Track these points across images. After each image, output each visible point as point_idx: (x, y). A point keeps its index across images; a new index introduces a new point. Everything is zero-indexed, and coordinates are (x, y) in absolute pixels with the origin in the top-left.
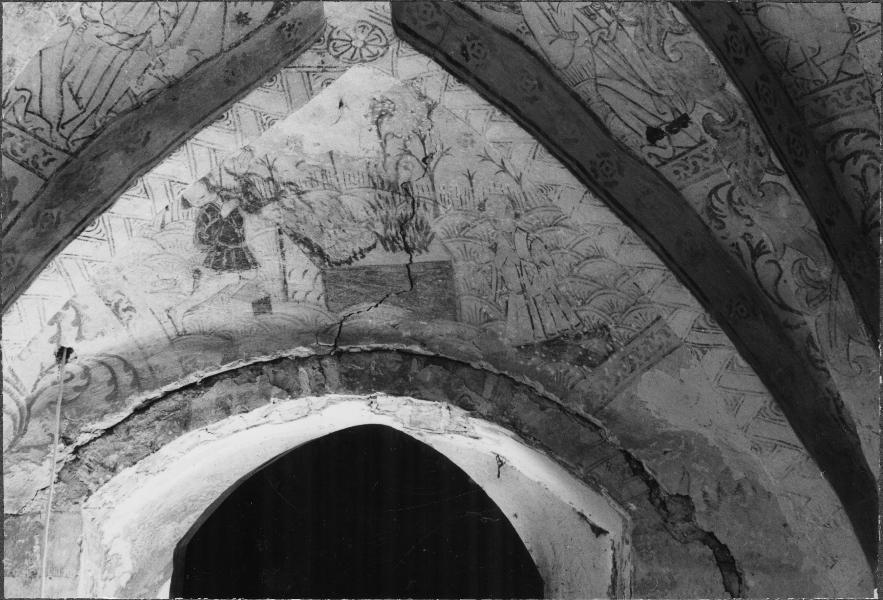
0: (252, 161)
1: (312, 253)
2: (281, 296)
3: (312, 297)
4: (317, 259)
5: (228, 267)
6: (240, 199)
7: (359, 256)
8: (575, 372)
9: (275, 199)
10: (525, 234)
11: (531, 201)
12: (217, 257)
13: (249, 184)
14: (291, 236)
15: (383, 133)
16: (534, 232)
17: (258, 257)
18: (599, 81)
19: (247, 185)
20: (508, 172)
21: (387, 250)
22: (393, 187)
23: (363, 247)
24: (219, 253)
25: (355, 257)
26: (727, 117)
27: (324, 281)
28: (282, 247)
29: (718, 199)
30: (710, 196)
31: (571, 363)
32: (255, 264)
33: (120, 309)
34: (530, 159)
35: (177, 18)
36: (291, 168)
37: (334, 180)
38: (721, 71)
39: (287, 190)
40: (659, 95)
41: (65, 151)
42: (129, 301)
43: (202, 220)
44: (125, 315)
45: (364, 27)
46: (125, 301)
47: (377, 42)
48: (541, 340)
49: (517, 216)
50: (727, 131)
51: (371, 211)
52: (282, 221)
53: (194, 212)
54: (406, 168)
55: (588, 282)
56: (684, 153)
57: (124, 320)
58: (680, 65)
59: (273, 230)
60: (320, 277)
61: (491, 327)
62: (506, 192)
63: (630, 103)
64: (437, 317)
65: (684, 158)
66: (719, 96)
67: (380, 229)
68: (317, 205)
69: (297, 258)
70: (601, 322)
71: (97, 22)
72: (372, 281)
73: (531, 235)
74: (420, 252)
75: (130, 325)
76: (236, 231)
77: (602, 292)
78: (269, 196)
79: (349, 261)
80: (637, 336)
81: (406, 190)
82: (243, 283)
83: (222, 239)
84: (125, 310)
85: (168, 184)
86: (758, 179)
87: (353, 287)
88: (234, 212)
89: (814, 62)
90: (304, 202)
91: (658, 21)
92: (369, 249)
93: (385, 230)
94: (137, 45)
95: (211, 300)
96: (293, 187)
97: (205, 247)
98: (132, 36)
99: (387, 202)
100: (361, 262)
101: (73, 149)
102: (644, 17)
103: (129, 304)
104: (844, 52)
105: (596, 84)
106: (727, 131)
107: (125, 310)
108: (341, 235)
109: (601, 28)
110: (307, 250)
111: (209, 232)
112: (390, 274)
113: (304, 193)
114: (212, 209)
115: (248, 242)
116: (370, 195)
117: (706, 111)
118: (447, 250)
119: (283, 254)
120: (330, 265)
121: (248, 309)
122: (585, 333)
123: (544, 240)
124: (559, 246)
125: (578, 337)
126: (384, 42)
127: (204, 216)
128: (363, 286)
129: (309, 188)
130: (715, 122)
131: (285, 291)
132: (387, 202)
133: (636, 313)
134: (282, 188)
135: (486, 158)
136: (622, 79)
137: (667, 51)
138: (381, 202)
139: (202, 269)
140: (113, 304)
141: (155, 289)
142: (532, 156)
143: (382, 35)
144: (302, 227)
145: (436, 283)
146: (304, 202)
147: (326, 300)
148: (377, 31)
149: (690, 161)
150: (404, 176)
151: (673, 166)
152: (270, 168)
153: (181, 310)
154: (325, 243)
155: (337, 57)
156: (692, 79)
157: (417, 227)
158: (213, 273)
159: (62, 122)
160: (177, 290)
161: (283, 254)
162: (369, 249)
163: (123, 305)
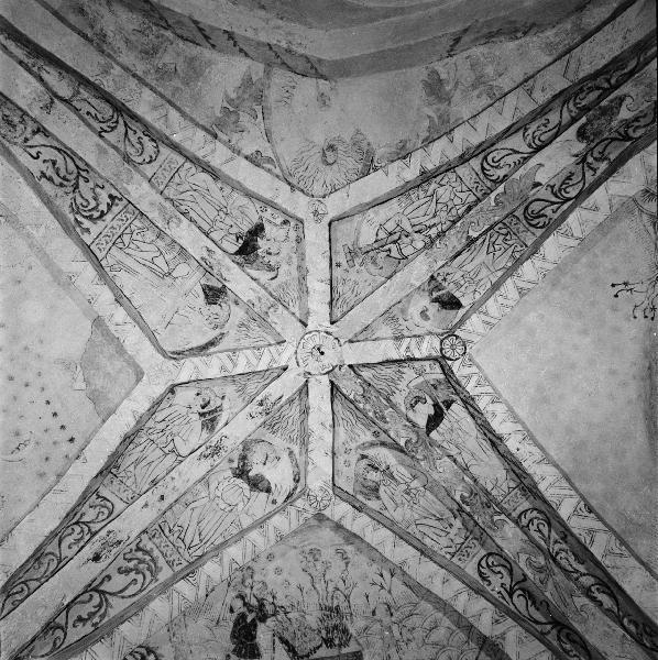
19: (262, 605)
22: (331, 609)
43: (236, 623)
53: (235, 615)
59: (271, 633)
79: (308, 656)
86: (492, 520)
88: (253, 620)
115: (257, 640)
118: (359, 644)
136: (425, 518)
152: (274, 597)
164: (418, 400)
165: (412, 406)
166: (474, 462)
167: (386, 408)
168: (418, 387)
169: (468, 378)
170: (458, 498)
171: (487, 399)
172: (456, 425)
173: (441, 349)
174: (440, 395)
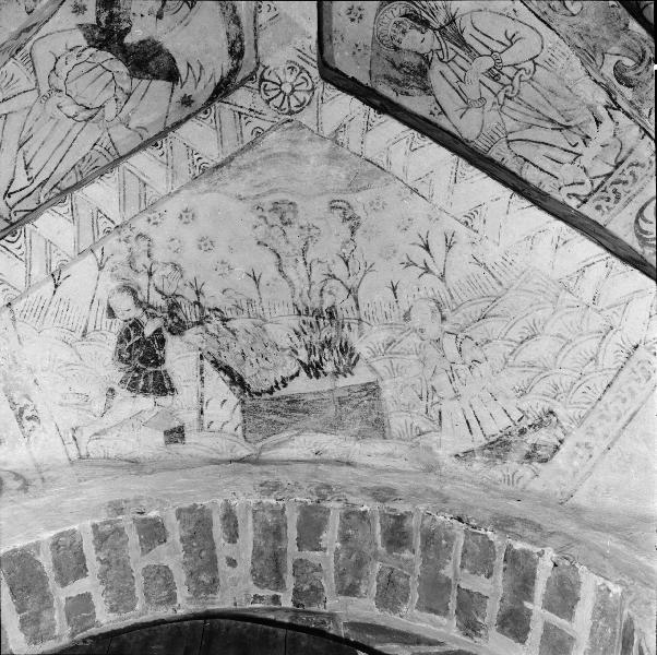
0: (181, 283)
1: (233, 382)
2: (196, 425)
3: (229, 428)
4: (238, 389)
5: (144, 391)
6: (166, 320)
7: (280, 385)
8: (526, 471)
9: (199, 323)
10: (454, 337)
11: (456, 298)
12: (134, 378)
13: (175, 305)
14: (212, 362)
15: (308, 262)
16: (462, 331)
17: (177, 382)
18: (510, 137)
20: (431, 272)
21: (311, 377)
23: (285, 376)
24: (136, 375)
25: (277, 386)
27: (243, 412)
28: (201, 373)
29: (646, 221)
30: (637, 222)
31: (518, 462)
32: (173, 390)
33: (24, 416)
34: (452, 185)
35: (129, 95)
36: (218, 293)
37: (259, 309)
38: (621, 10)
39: (212, 315)
40: (568, 127)
41: (6, 220)
42: (35, 409)
43: (125, 336)
44: (28, 424)
45: (293, 68)
46: (31, 408)
47: (303, 87)
48: (481, 444)
49: (443, 319)
51: (295, 338)
52: (204, 346)
53: (118, 326)
54: (330, 293)
55: (526, 369)
56: (603, 183)
57: (26, 430)
58: (582, 17)
60: (239, 408)
61: (423, 441)
62: (431, 294)
63: (542, 146)
64: (363, 437)
65: (603, 189)
67: (303, 355)
68: (241, 333)
69: (217, 384)
70: (546, 409)
71: (61, 91)
72: (294, 410)
73: (459, 336)
74: (345, 376)
75: (31, 438)
76: (157, 352)
77: (542, 375)
78: (194, 320)
79: (271, 391)
80: (589, 412)
81: (331, 313)
82: (157, 409)
83: (142, 360)
84: (29, 419)
85: (95, 212)
87: (274, 417)
88: (158, 331)
90: (228, 329)
92: (292, 378)
93: (309, 356)
94: (91, 118)
95: (120, 425)
96: (218, 313)
97: (123, 366)
98: (88, 108)
99: (311, 326)
100: (284, 392)
101: (14, 219)
103: (34, 413)
105: (508, 142)
107: (29, 419)
108: (263, 363)
109: (505, 86)
110: (227, 378)
111: (129, 350)
112: (313, 401)
113: (228, 320)
114: (136, 325)
115: (167, 366)
116: (295, 322)
117: (617, 58)
119: (202, 379)
120: (250, 395)
121: (161, 438)
122: (530, 426)
123: (473, 337)
124: (491, 338)
125: (522, 432)
126: (310, 87)
127: (127, 331)
128: (285, 416)
129: (235, 315)
130: (626, 69)
131: (200, 421)
132: (311, 326)
133: (583, 388)
134: (208, 313)
135: (410, 264)
138: (305, 327)
139: (117, 388)
140: (18, 407)
141: (65, 402)
142: (453, 179)
143: (308, 77)
144: (223, 354)
145: (362, 405)
146: (228, 329)
147: (244, 430)
148: (305, 75)
149: (610, 190)
150: (328, 301)
151: (595, 200)
152: (197, 293)
153: (88, 433)
154: (247, 373)
155: (268, 102)
156: (596, 29)
157: (341, 350)
158: (129, 394)
159: (10, 191)
160: (87, 407)
161: (202, 379)
162: (292, 378)
163: (27, 413)
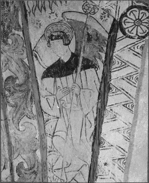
26: (30, 166)
50: (26, 174)
58: (22, 134)
66: (30, 155)
89: (65, 170)
91: (24, 108)
102: (19, 104)
104: (79, 170)
106: (26, 174)
117: (22, 160)
137: (20, 124)
164: (64, 37)
165: (51, 37)
166: (63, 135)
167: (18, 28)
168: (73, 24)
169: (124, 64)
170: (16, 163)
171: (123, 98)
172: (76, 90)
173: (124, 15)
174: (87, 50)
